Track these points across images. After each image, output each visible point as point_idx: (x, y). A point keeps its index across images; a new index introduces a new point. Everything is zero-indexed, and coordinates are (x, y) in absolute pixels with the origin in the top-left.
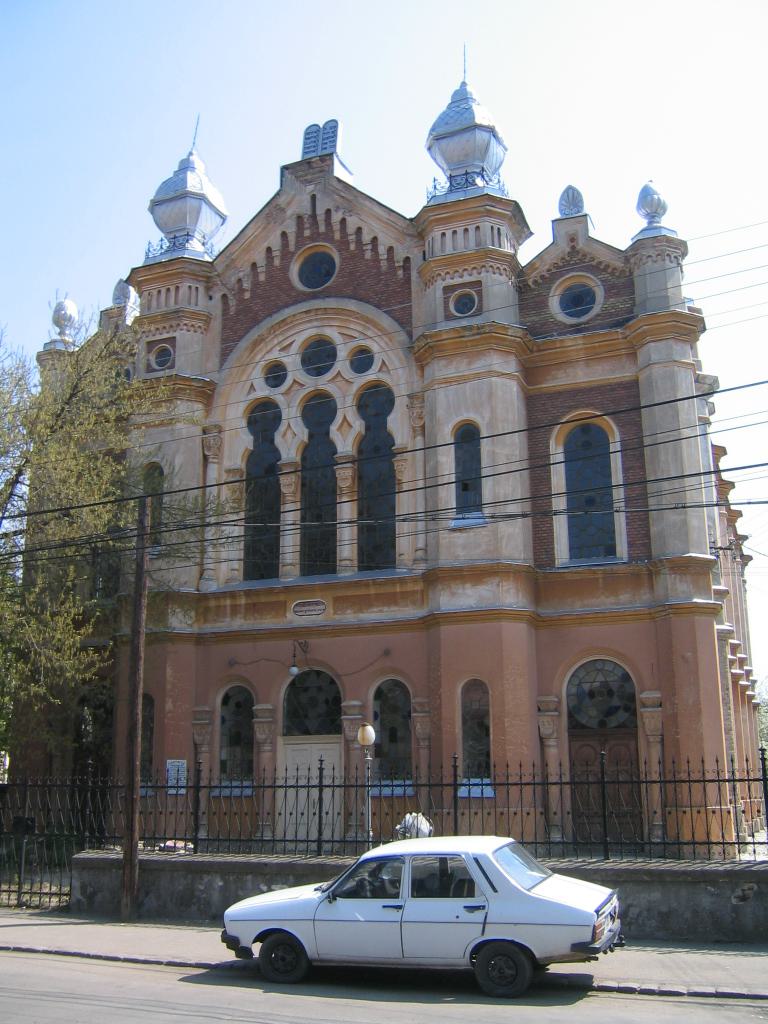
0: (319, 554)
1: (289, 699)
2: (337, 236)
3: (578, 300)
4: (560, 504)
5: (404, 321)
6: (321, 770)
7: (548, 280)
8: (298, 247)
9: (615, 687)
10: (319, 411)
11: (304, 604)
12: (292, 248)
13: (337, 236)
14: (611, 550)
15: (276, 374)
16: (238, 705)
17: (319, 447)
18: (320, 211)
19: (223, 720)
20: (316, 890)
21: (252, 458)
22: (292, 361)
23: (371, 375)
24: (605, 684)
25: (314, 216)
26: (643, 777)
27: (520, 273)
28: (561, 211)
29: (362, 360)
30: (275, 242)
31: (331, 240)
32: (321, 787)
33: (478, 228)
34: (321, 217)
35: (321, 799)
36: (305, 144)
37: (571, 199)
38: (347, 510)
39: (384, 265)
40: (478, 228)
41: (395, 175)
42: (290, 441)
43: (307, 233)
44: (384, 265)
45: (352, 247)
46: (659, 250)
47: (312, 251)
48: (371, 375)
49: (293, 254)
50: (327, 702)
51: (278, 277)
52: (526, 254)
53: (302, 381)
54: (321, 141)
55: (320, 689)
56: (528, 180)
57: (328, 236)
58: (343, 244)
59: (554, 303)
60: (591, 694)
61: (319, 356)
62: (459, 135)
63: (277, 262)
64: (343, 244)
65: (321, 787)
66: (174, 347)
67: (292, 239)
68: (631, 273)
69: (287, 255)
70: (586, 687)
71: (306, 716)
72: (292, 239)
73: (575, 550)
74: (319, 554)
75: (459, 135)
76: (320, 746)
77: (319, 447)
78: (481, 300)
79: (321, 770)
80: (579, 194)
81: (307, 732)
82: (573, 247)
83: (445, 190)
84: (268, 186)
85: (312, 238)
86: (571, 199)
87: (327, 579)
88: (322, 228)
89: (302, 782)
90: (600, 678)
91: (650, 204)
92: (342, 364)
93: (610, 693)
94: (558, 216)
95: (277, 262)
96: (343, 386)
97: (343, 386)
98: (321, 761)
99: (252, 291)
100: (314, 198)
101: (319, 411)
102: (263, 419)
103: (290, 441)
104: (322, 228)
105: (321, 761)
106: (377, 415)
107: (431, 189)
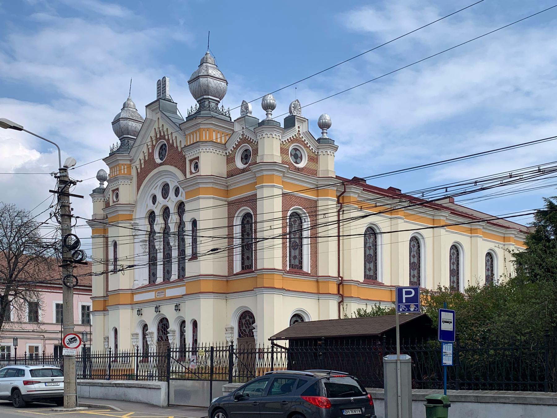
2: (166, 137)
12: (154, 143)
15: (154, 199)
43: (158, 136)
63: (150, 151)
69: (153, 147)
77: (166, 231)
85: (160, 139)
95: (150, 151)
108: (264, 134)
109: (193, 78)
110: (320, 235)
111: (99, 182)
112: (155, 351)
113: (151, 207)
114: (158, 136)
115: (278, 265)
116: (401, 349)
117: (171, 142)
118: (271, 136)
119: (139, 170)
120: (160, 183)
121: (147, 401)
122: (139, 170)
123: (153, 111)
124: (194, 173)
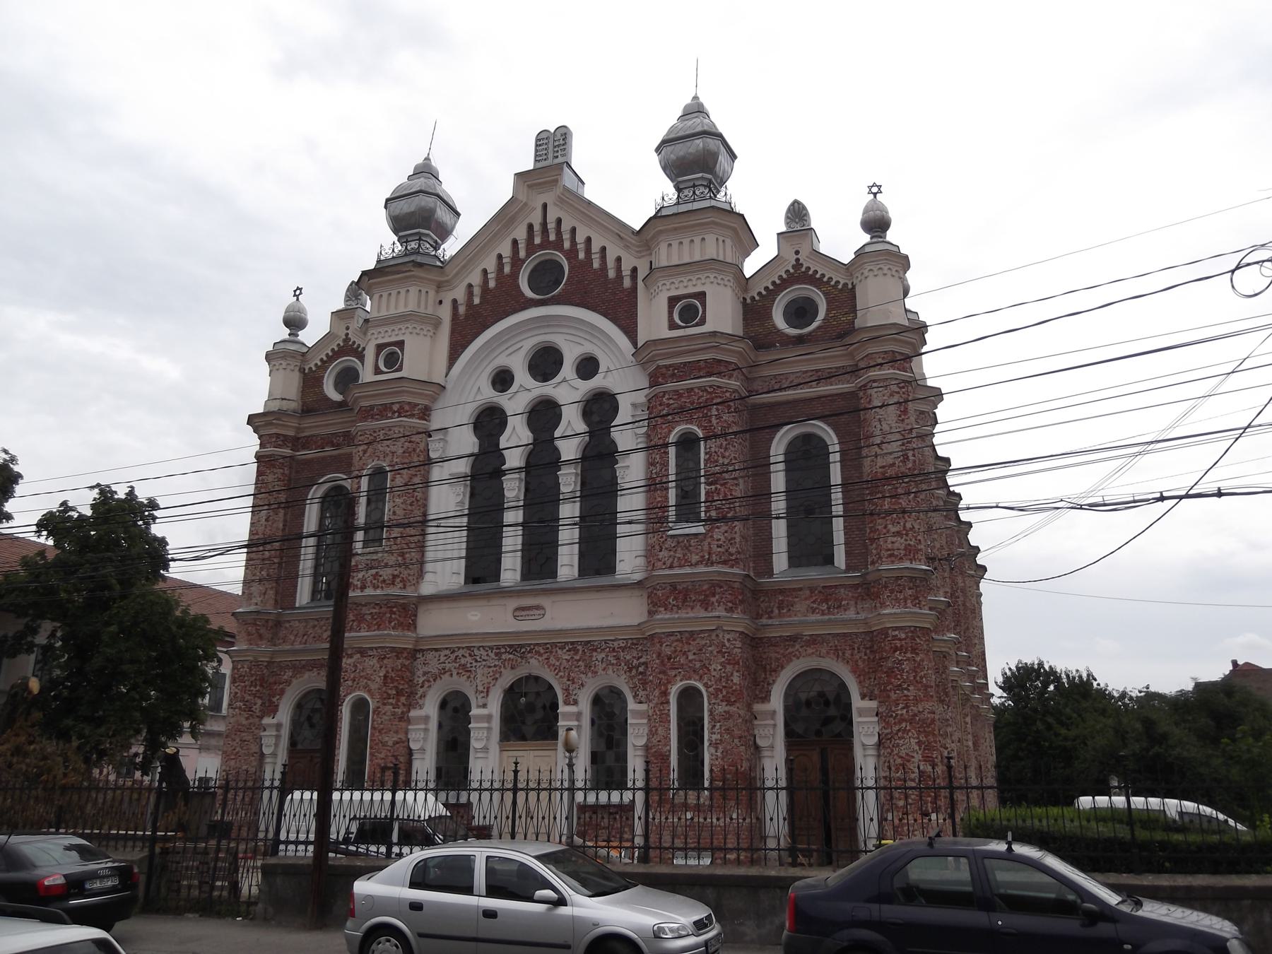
0: (540, 560)
1: (505, 706)
2: (567, 245)
3: (800, 312)
4: (779, 505)
5: (630, 331)
6: (516, 772)
7: (772, 293)
8: (528, 255)
9: (831, 697)
10: (544, 415)
11: (523, 609)
12: (522, 254)
13: (567, 245)
14: (829, 560)
15: (503, 380)
16: (456, 710)
17: (542, 460)
18: (551, 218)
19: (440, 726)
20: (69, 848)
21: (477, 458)
22: (519, 367)
23: (597, 382)
24: (821, 695)
25: (544, 224)
26: (858, 783)
27: (744, 283)
28: (787, 224)
29: (588, 367)
30: (506, 250)
32: (515, 790)
33: (703, 239)
34: (551, 226)
35: (514, 803)
36: (536, 151)
37: (797, 213)
38: (569, 510)
39: (612, 274)
40: (703, 239)
41: (628, 188)
42: (516, 439)
43: (537, 240)
44: (612, 274)
45: (581, 256)
46: (883, 257)
47: (542, 259)
48: (597, 382)
49: (523, 261)
50: (544, 707)
51: (507, 283)
52: (751, 266)
53: (526, 391)
54: (554, 146)
55: (538, 694)
56: (756, 195)
57: (558, 244)
58: (572, 254)
59: (779, 321)
60: (808, 703)
61: (545, 363)
62: (696, 156)
63: (507, 269)
64: (572, 254)
65: (515, 790)
66: (402, 350)
67: (522, 246)
68: (854, 287)
69: (517, 262)
70: (803, 696)
71: (523, 723)
72: (522, 246)
73: (795, 560)
74: (540, 560)
75: (696, 156)
76: (537, 753)
77: (542, 460)
78: (704, 311)
79: (516, 772)
80: (804, 208)
81: (523, 738)
82: (797, 260)
83: (674, 201)
84: (503, 192)
85: (542, 246)
86: (797, 213)
87: (547, 584)
88: (552, 237)
89: (496, 785)
90: (817, 688)
91: (876, 224)
92: (568, 370)
93: (827, 703)
94: (783, 229)
95: (507, 269)
96: (568, 391)
97: (568, 391)
98: (516, 763)
99: (482, 297)
100: (545, 206)
101: (544, 415)
102: (489, 422)
103: (516, 439)
104: (552, 237)
105: (516, 763)
106: (601, 422)
107: (659, 201)
109: (672, 136)
110: (639, 528)
111: (288, 331)
112: (496, 777)
113: (488, 394)
114: (537, 240)
115: (54, 674)
116: (471, 871)
117: (581, 256)
118: (889, 273)
119: (462, 310)
120: (529, 343)
121: (474, 935)
122: (462, 310)
123: (529, 186)
124: (680, 327)
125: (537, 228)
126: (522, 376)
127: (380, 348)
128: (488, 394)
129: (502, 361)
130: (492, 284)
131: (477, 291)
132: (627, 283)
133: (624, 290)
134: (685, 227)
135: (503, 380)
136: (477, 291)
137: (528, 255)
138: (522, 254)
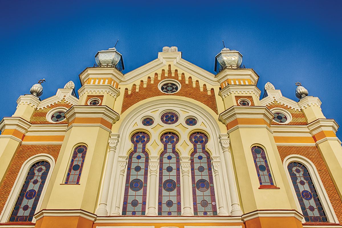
2: (180, 78)
5: (214, 108)
10: (170, 138)
12: (159, 78)
13: (180, 78)
15: (191, 121)
22: (157, 118)
23: (64, 97)
29: (148, 121)
31: (177, 79)
43: (166, 75)
45: (187, 82)
49: (160, 81)
63: (152, 82)
64: (183, 81)
88: (173, 75)
95: (152, 82)
101: (170, 138)
102: (140, 138)
104: (173, 75)
108: (85, 91)
120: (163, 109)
125: (166, 71)
126: (157, 120)
127: (89, 97)
128: (141, 126)
129: (148, 113)
130: (145, 86)
131: (138, 87)
132: (209, 93)
133: (207, 95)
134: (186, 105)
135: (191, 121)
136: (138, 87)
137: (162, 80)
138: (159, 78)
